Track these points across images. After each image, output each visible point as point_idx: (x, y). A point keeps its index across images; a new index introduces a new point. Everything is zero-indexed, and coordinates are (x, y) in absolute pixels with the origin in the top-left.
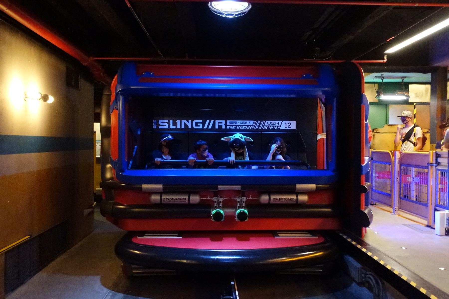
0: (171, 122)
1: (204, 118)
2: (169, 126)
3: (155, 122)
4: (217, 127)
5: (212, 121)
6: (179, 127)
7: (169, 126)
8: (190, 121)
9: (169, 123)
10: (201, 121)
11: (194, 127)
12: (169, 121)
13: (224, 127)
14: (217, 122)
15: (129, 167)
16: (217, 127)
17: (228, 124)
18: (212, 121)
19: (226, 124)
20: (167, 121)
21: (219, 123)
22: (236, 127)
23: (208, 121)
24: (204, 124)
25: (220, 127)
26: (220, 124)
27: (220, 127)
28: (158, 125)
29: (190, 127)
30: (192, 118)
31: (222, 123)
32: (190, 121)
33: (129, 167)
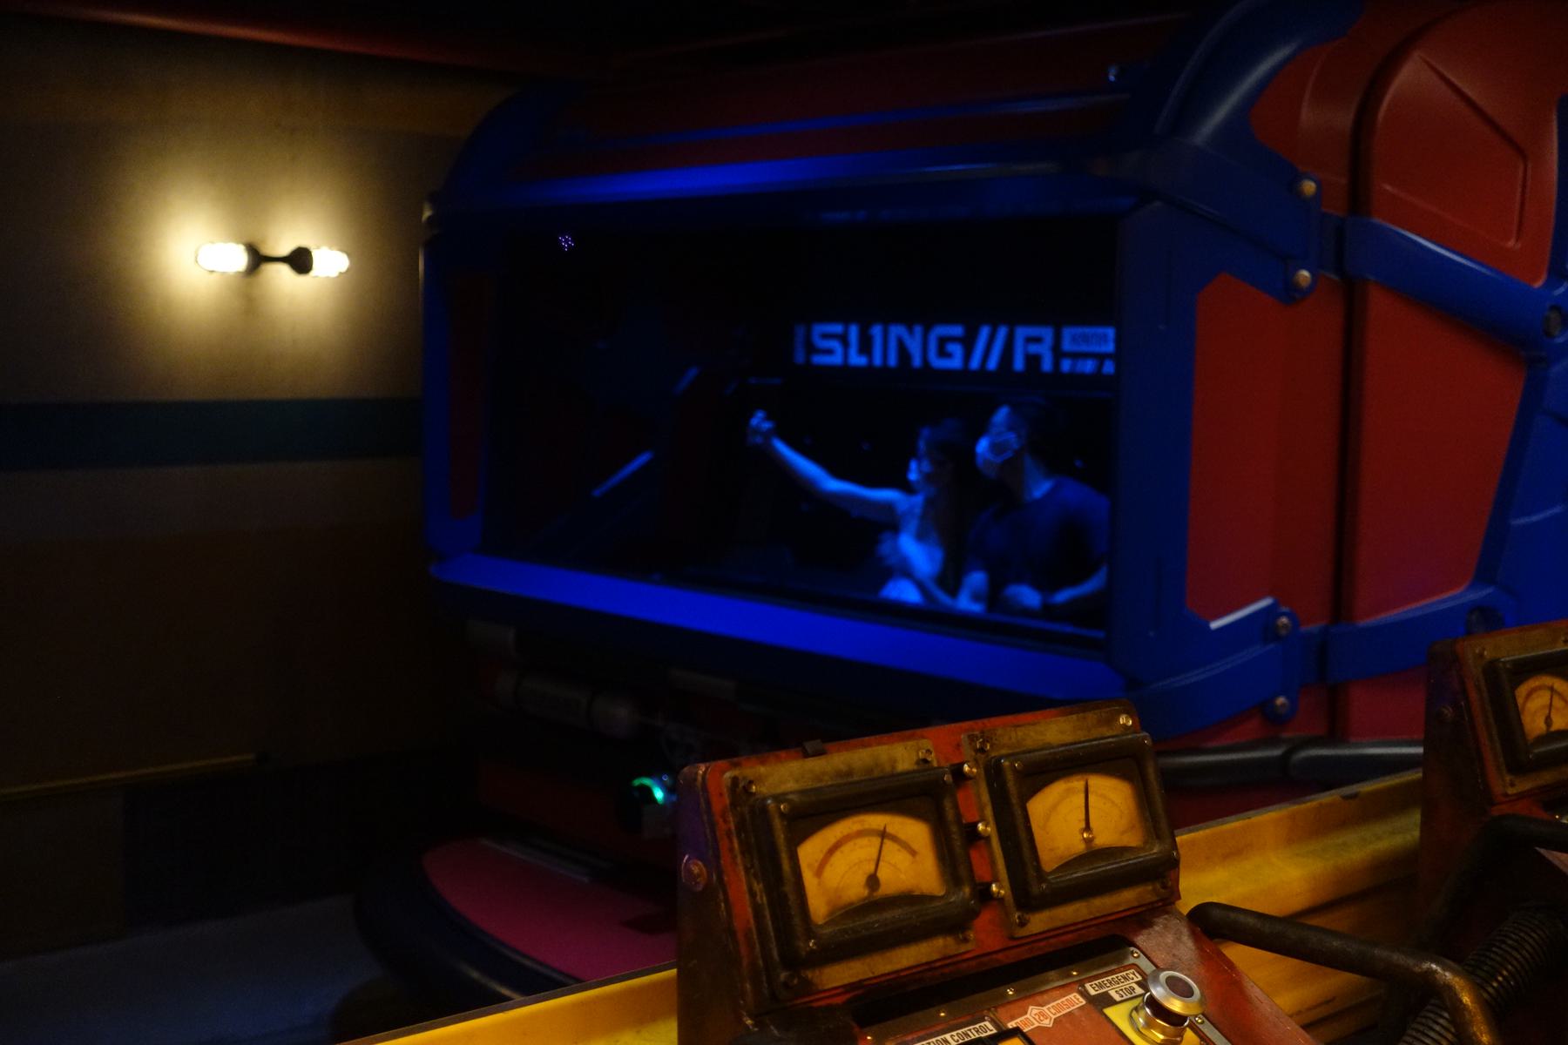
0: (854, 332)
1: (971, 316)
2: (846, 355)
3: (800, 331)
4: (1019, 364)
5: (1002, 332)
6: (878, 361)
7: (846, 355)
8: (918, 330)
9: (844, 339)
10: (957, 331)
11: (939, 363)
12: (1056, 364)
13: (1047, 365)
14: (1021, 333)
15: (1101, 635)
16: (1019, 364)
17: (1067, 345)
18: (1002, 332)
19: (1058, 353)
20: (838, 328)
21: (1030, 340)
22: (1101, 365)
23: (985, 332)
24: (968, 343)
25: (1033, 361)
26: (1033, 349)
27: (1033, 361)
28: (811, 349)
29: (917, 362)
30: (921, 314)
31: (1038, 340)
32: (918, 330)
33: (1101, 635)
